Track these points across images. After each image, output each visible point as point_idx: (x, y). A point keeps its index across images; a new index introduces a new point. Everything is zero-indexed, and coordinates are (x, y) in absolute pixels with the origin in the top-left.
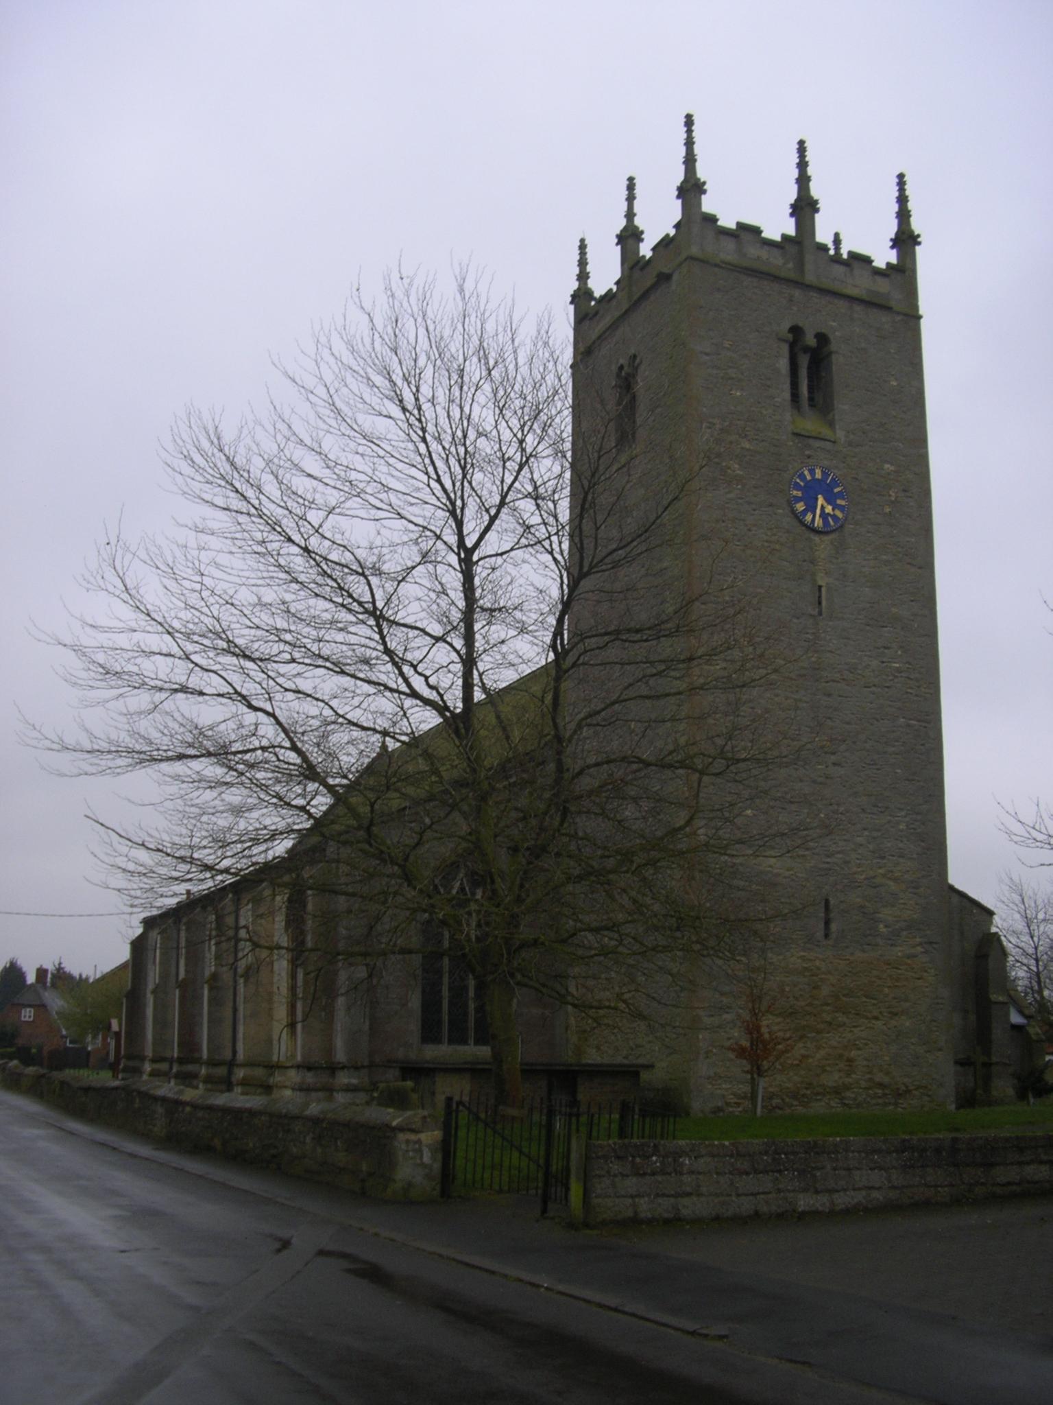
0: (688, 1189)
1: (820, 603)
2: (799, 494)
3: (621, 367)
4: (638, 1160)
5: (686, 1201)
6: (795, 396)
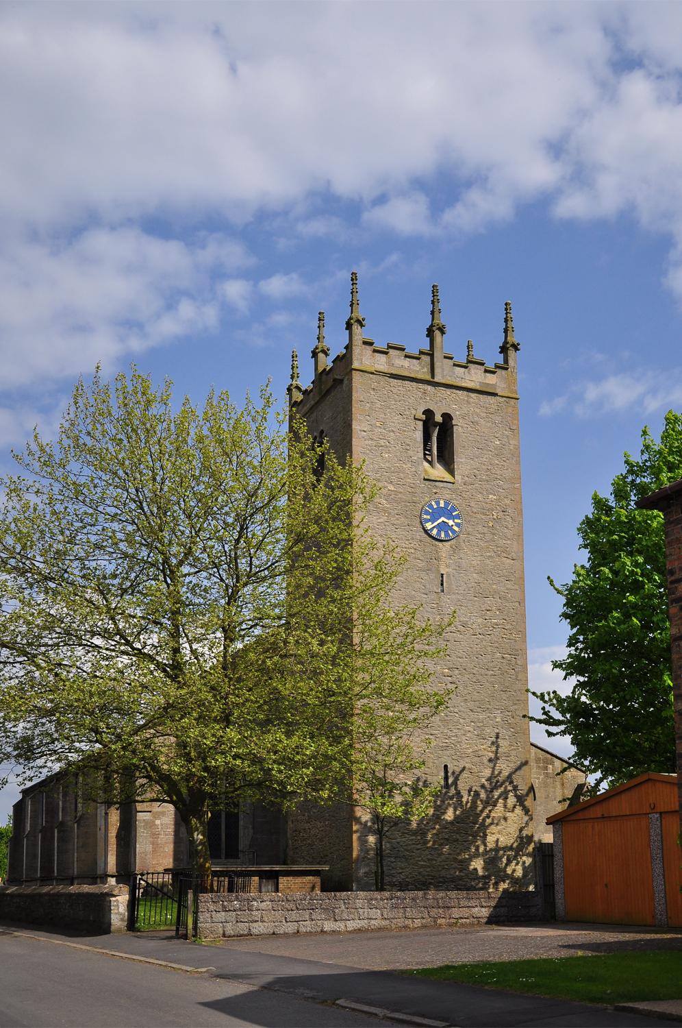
0: (256, 919)
1: (442, 584)
2: (429, 517)
4: (225, 903)
5: (255, 925)
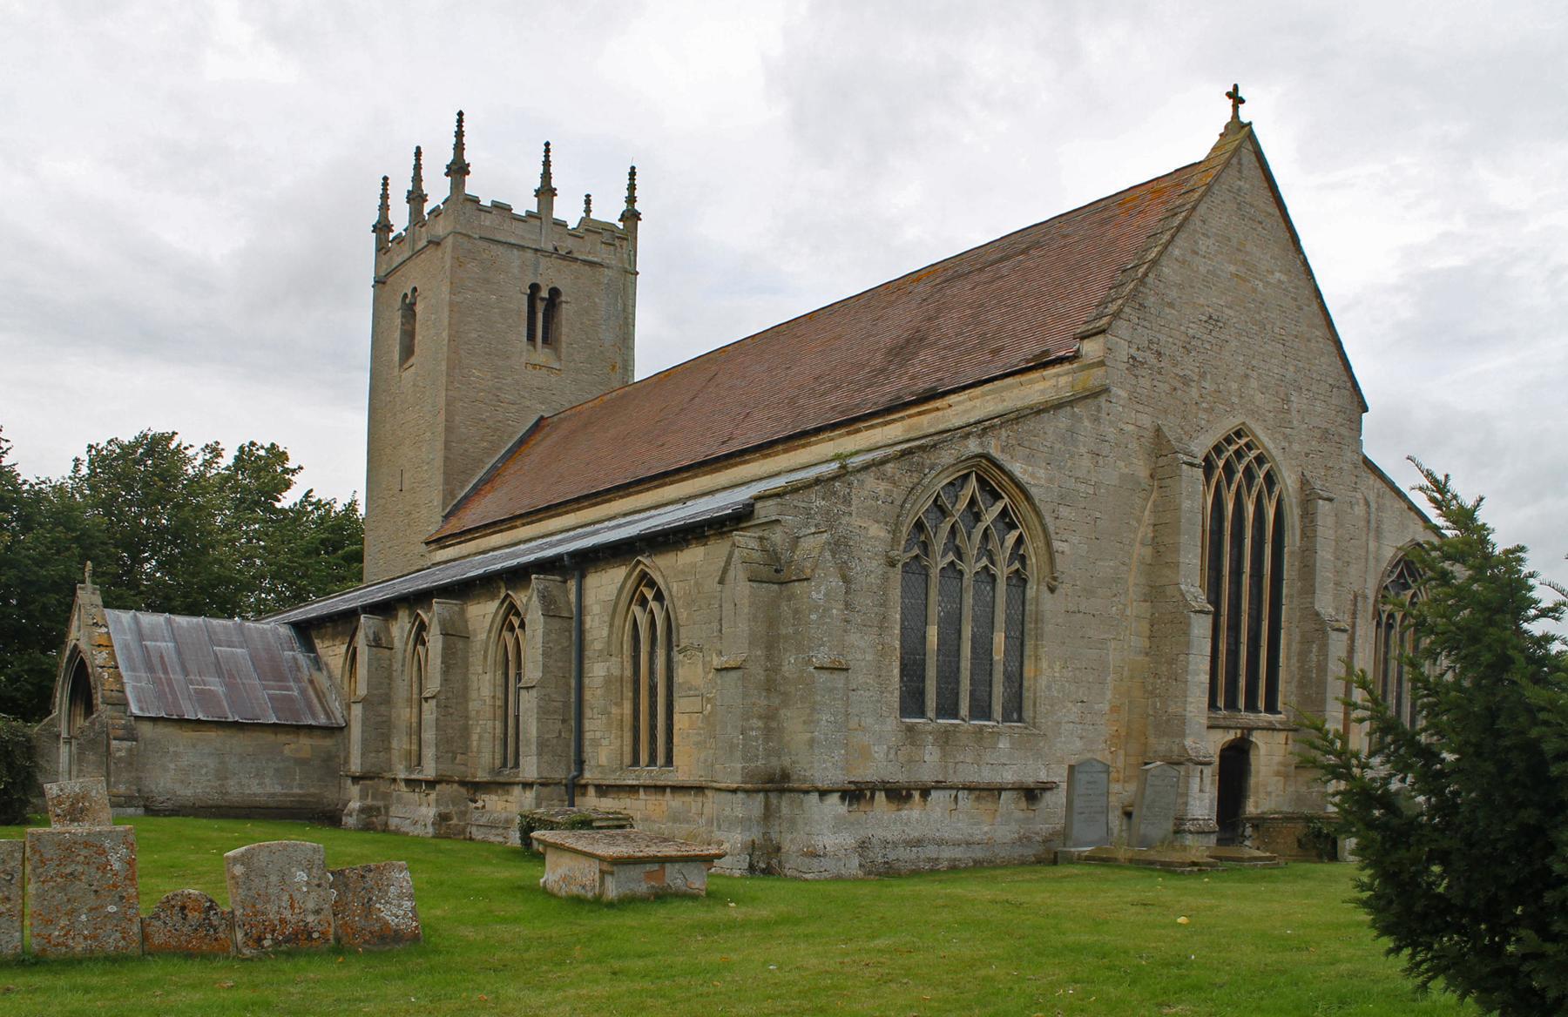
3: (406, 296)
6: (531, 337)
